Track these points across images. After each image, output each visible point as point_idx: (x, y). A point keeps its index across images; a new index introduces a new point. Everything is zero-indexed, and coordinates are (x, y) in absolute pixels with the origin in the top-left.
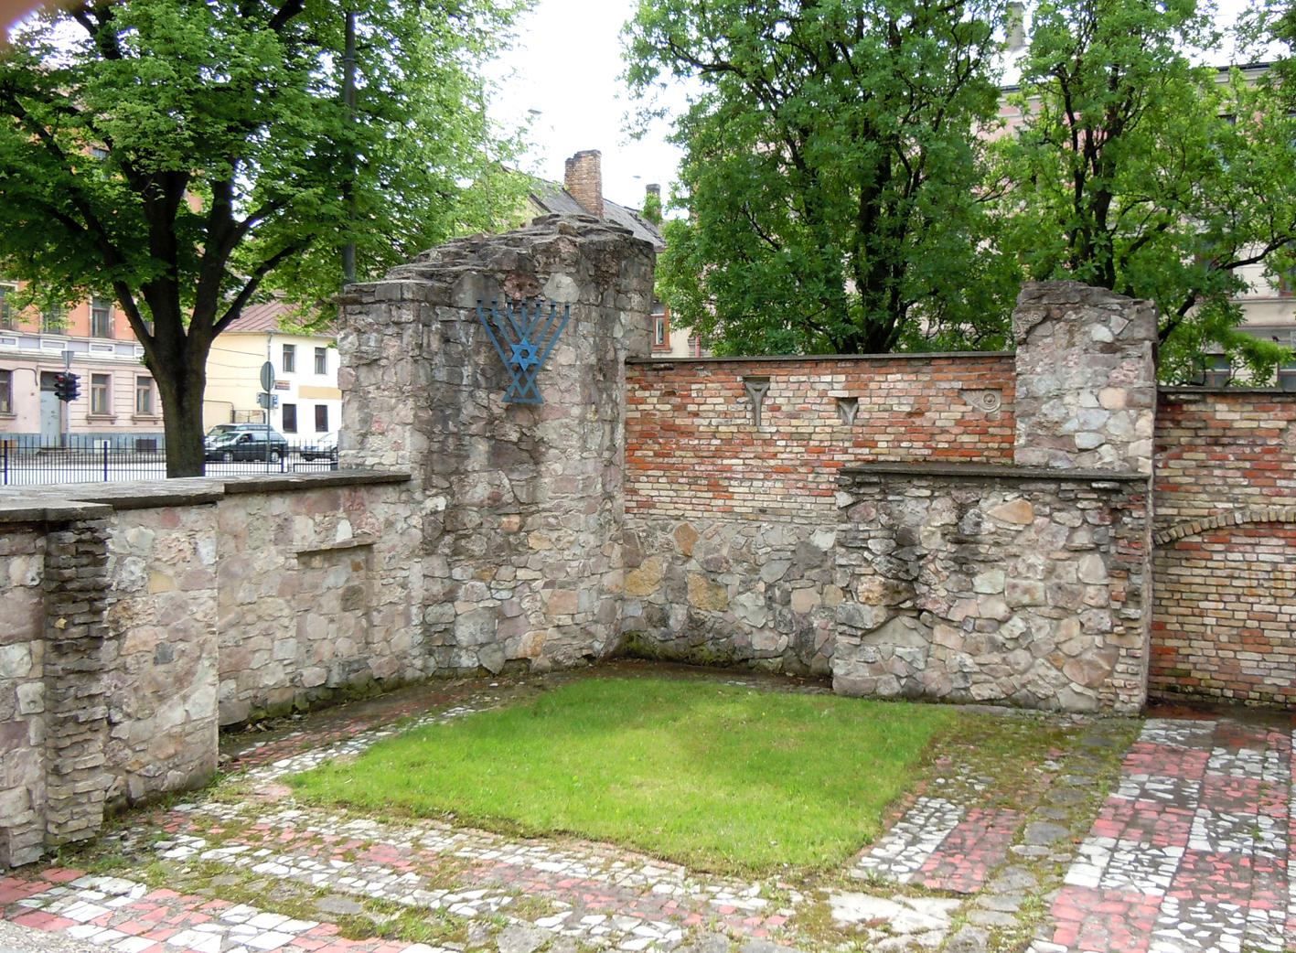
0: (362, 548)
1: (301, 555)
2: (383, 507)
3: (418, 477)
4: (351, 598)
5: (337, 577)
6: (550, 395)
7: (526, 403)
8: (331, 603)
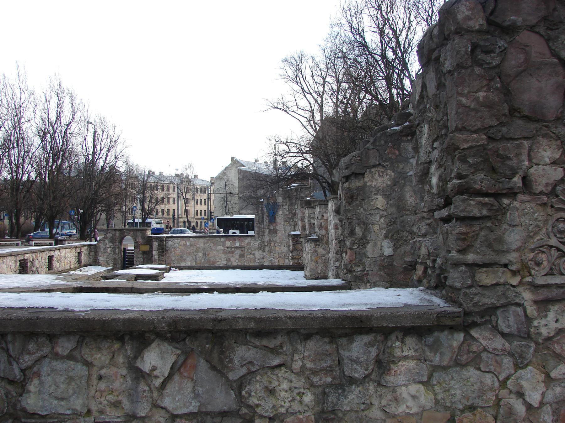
4: (242, 256)
5: (238, 252)
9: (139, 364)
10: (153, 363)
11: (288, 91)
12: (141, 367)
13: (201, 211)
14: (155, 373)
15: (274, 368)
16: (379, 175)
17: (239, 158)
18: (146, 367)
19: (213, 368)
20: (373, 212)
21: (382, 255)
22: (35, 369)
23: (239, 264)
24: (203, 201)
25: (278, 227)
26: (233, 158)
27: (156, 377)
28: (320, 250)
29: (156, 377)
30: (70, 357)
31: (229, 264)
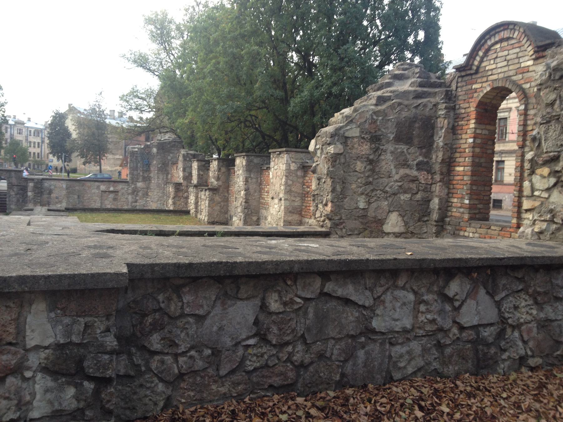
0: (115, 192)
1: (102, 191)
2: (120, 187)
3: (130, 182)
4: (115, 199)
5: (112, 196)
6: (152, 169)
7: (148, 170)
8: (111, 199)
9: (446, 292)
10: (456, 290)
11: (149, 48)
12: (448, 294)
13: (34, 153)
14: (457, 297)
15: (518, 291)
16: (359, 145)
17: (75, 105)
18: (451, 294)
19: (488, 293)
20: (352, 174)
21: (357, 208)
22: (382, 298)
23: (113, 207)
24: (37, 144)
25: (152, 175)
26: (70, 105)
27: (457, 300)
28: (217, 198)
29: (457, 300)
30: (403, 288)
31: (104, 207)
